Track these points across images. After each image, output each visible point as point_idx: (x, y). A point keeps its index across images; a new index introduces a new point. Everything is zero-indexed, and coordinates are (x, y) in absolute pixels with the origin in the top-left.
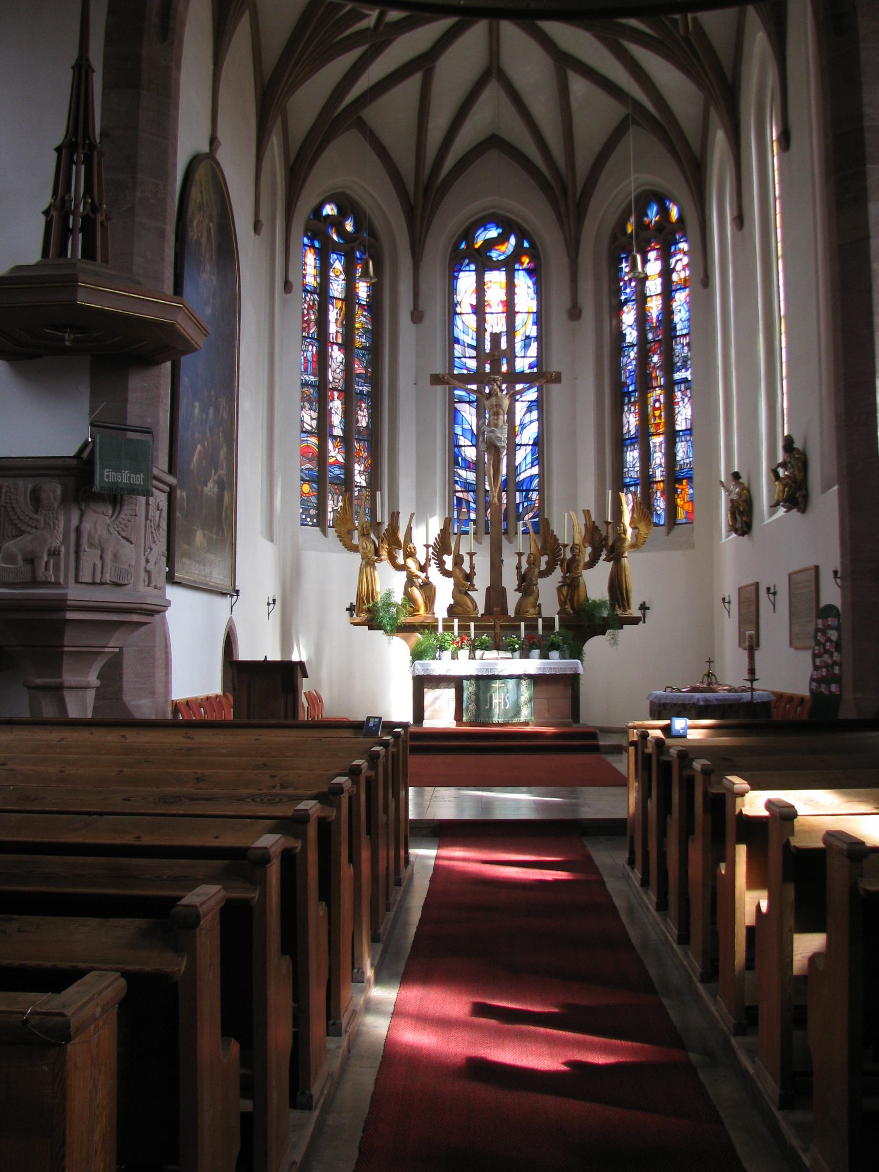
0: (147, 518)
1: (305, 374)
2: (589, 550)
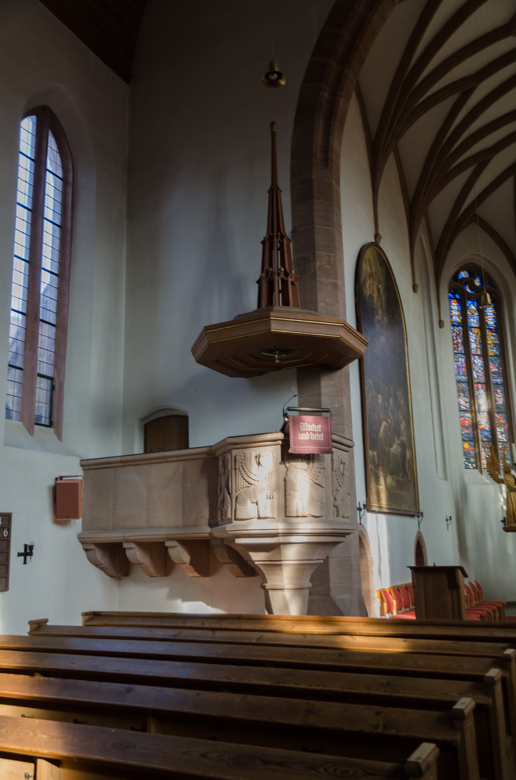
0: (333, 470)
1: (459, 376)
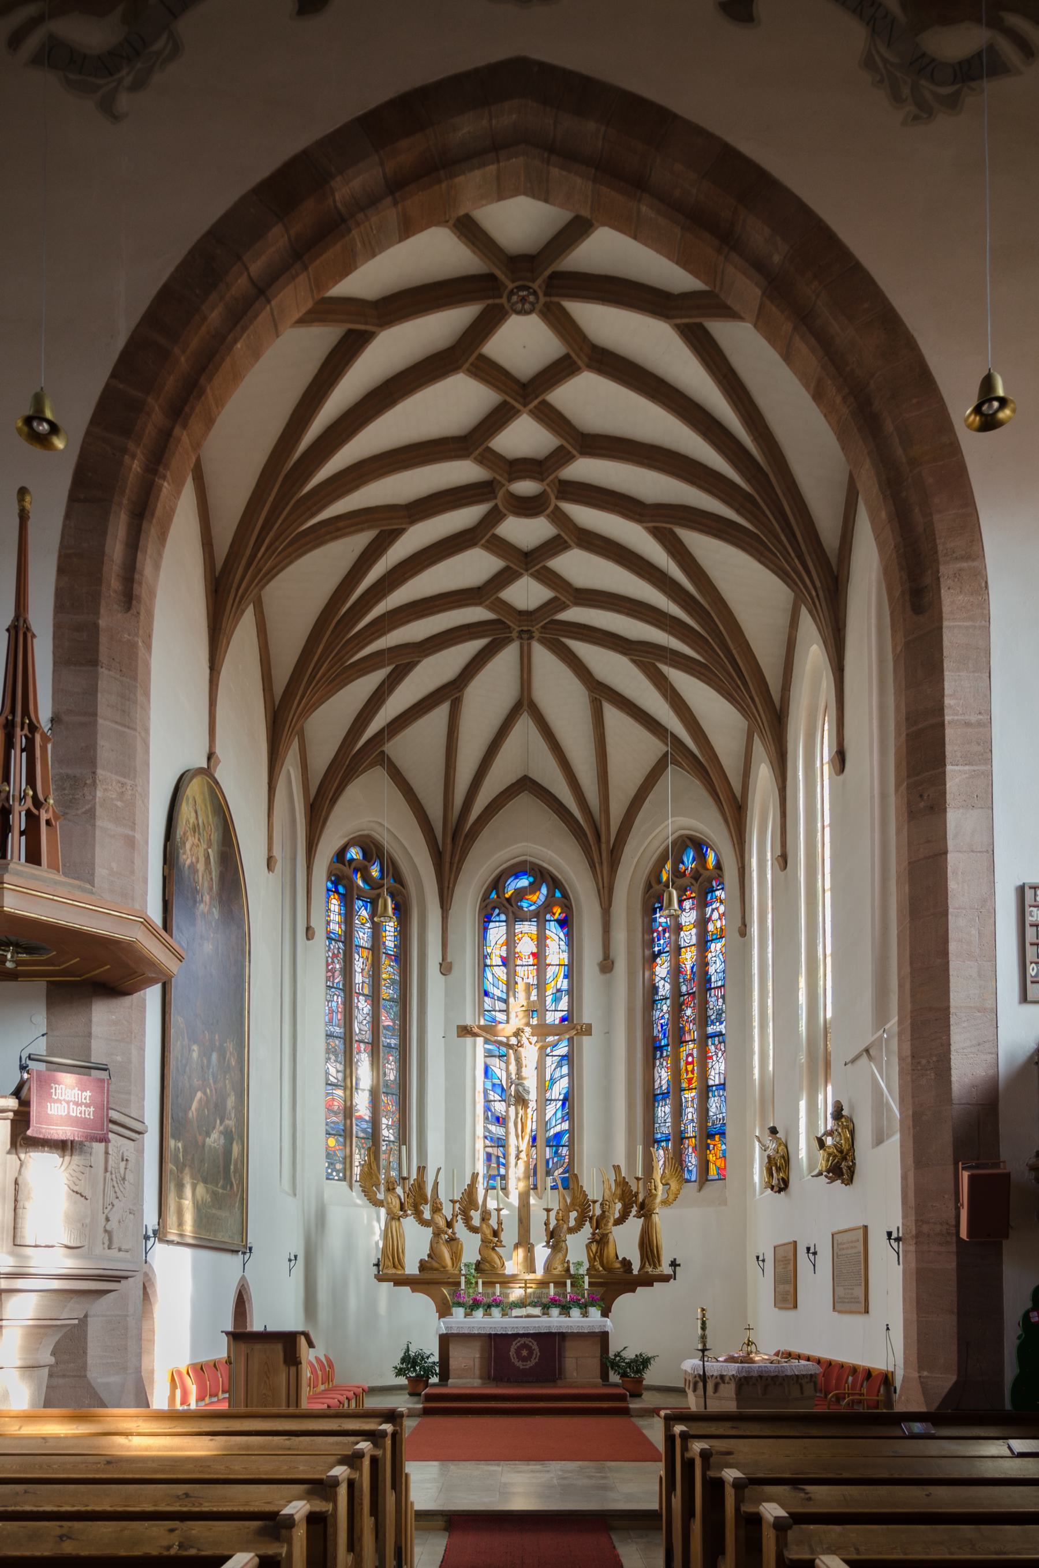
0: (106, 1170)
2: (619, 1206)
